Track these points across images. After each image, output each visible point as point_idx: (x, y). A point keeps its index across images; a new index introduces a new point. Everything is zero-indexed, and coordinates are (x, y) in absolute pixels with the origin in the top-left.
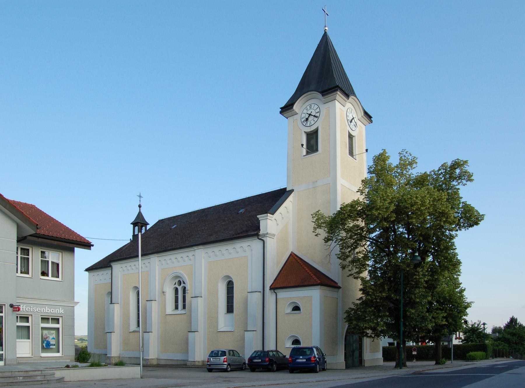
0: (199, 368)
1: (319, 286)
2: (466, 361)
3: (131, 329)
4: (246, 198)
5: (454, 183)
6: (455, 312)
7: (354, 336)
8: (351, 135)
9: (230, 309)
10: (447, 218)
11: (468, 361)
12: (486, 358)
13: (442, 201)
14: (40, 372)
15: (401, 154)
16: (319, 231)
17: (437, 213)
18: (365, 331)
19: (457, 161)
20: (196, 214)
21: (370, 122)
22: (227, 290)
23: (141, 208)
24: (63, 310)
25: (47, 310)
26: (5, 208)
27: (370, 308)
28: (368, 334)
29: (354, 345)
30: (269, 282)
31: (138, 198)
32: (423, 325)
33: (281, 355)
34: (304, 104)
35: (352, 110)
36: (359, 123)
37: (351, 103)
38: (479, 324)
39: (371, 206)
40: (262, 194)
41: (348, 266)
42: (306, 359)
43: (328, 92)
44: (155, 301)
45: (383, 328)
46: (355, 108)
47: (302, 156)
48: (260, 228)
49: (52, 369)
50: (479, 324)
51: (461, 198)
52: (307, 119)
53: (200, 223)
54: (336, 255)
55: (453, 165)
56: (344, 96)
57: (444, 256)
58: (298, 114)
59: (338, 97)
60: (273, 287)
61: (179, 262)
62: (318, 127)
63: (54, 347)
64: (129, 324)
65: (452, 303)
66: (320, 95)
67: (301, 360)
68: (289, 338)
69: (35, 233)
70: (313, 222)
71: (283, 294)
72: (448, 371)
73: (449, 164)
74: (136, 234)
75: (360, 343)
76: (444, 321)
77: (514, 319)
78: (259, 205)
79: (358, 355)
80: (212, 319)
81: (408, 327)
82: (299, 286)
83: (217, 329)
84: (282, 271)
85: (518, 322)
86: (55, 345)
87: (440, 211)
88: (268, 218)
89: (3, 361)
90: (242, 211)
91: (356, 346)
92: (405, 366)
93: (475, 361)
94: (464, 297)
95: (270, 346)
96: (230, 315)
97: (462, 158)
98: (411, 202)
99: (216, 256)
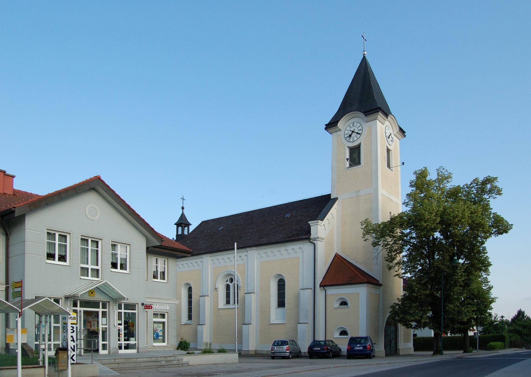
1: (366, 284)
2: (487, 351)
3: (182, 322)
4: (289, 203)
5: (486, 196)
6: (482, 307)
7: (391, 327)
8: (389, 149)
9: (281, 303)
10: (483, 228)
12: (504, 348)
13: (478, 213)
14: (174, 358)
15: (439, 170)
16: (368, 236)
17: (475, 224)
18: (410, 323)
19: (488, 177)
22: (278, 287)
24: (169, 307)
26: (141, 225)
27: (415, 303)
28: (412, 325)
29: (391, 335)
30: (319, 280)
32: (460, 318)
33: (334, 345)
34: (347, 122)
36: (395, 138)
38: (496, 317)
39: (419, 218)
40: (304, 200)
41: (394, 267)
42: (363, 347)
45: (426, 321)
46: (391, 124)
47: (346, 168)
48: (311, 233)
49: (181, 355)
50: (496, 317)
51: (491, 209)
52: (350, 136)
53: (247, 226)
54: (385, 258)
55: (485, 181)
56: (384, 116)
57: (477, 259)
58: (341, 130)
59: (379, 117)
60: (323, 285)
63: (161, 338)
64: (181, 317)
65: (479, 298)
66: (362, 115)
67: (358, 348)
68: (337, 329)
69: (160, 244)
70: (362, 228)
71: (332, 291)
72: (488, 356)
73: (481, 179)
74: (179, 234)
75: (396, 333)
76: (474, 314)
77: (522, 312)
78: (304, 210)
79: (394, 345)
80: (264, 312)
83: (270, 322)
84: (329, 271)
85: (525, 315)
87: (477, 222)
88: (319, 224)
89: (107, 350)
90: (288, 215)
92: (442, 354)
93: (496, 350)
94: (490, 293)
95: (321, 337)
96: (281, 309)
97: (493, 175)
98: (454, 215)
99: (268, 256)
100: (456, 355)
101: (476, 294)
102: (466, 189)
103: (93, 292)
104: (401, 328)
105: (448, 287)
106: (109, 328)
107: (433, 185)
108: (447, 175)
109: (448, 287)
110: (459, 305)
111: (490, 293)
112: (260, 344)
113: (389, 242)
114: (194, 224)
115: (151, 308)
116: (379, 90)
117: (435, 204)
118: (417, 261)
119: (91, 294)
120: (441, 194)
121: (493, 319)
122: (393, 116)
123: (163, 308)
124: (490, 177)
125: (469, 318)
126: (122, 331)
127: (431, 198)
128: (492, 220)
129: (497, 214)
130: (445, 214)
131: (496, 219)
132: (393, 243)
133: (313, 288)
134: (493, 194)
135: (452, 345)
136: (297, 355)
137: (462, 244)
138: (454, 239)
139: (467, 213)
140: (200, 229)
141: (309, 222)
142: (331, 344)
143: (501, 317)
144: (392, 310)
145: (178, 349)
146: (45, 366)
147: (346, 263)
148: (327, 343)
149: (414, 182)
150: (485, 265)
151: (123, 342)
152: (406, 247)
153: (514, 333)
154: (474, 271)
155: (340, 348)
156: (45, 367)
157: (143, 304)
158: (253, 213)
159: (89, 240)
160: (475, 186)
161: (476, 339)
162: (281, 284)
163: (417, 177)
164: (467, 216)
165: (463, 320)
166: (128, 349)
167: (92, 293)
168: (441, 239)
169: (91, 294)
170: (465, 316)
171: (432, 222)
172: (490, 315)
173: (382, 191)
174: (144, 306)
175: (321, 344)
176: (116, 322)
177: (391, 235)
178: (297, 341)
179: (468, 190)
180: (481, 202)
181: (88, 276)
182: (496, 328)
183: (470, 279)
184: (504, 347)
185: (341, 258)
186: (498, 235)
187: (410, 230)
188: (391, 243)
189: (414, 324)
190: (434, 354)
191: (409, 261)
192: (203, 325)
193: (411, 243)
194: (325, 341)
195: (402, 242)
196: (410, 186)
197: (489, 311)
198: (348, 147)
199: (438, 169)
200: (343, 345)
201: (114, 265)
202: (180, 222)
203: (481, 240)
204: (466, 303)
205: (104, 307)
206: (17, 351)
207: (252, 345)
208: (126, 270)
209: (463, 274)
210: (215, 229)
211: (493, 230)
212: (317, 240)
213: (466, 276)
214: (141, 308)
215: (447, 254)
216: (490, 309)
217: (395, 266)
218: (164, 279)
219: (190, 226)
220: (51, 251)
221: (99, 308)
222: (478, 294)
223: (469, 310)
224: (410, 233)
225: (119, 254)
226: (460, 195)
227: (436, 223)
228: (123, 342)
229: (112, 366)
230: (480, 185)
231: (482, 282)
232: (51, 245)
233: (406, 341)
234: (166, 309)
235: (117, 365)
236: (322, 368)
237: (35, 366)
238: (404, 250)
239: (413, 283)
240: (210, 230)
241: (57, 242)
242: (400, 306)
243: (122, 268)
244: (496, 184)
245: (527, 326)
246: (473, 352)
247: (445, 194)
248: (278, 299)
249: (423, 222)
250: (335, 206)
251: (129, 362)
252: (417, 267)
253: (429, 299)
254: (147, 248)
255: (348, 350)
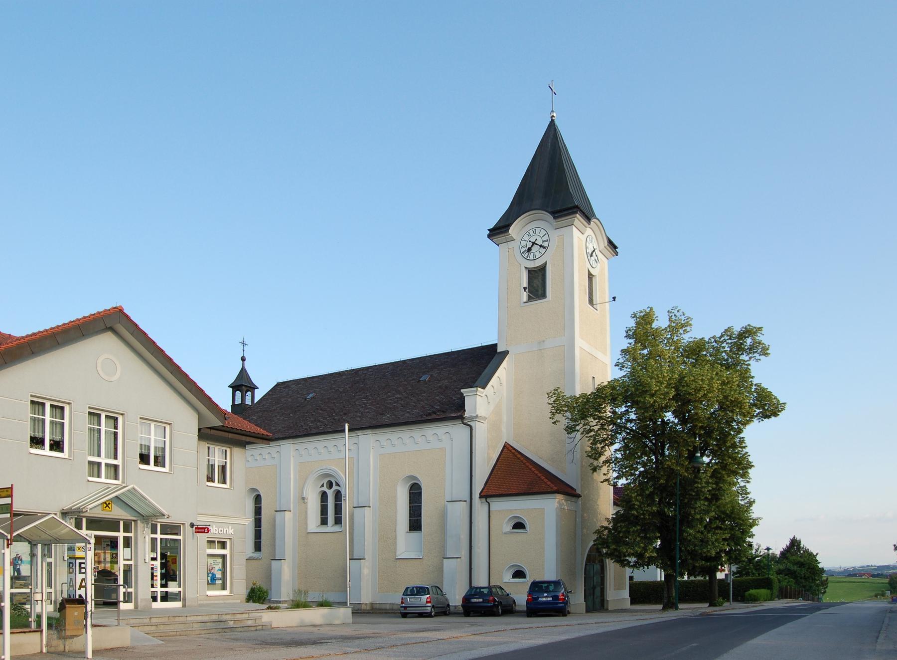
0: (370, 613)
5: (744, 357)
6: (738, 534)
7: (595, 565)
8: (591, 274)
9: (415, 525)
10: (741, 408)
11: (747, 602)
14: (247, 615)
16: (558, 417)
19: (748, 327)
20: (344, 377)
21: (615, 253)
23: (245, 362)
24: (232, 530)
25: (214, 530)
27: (635, 526)
28: (630, 562)
29: (595, 578)
30: (478, 487)
31: (241, 346)
32: (705, 550)
35: (592, 238)
36: (600, 256)
37: (592, 229)
38: (758, 549)
43: (562, 214)
44: (290, 512)
46: (594, 233)
50: (758, 549)
51: (753, 377)
52: (529, 250)
53: (357, 393)
54: (586, 452)
56: (584, 220)
59: (576, 222)
60: (485, 494)
61: (330, 452)
62: (546, 262)
63: (220, 582)
65: (734, 519)
66: (549, 217)
67: (545, 598)
69: (222, 425)
70: (549, 403)
71: (499, 505)
72: (746, 611)
73: (737, 329)
74: (236, 403)
75: (602, 575)
76: (726, 544)
77: (796, 540)
78: (452, 369)
80: (387, 540)
81: (683, 553)
82: (524, 493)
85: (802, 546)
86: (221, 580)
87: (732, 399)
88: (478, 394)
90: (426, 377)
91: (597, 579)
92: (677, 608)
93: (759, 602)
94: (750, 511)
95: (481, 581)
96: (415, 535)
98: (696, 386)
100: (699, 610)
101: (728, 512)
102: (714, 344)
103: (109, 503)
104: (611, 565)
105: (686, 500)
106: (136, 566)
107: (662, 336)
108: (684, 320)
109: (686, 500)
110: (703, 529)
111: (750, 511)
112: (379, 592)
113: (593, 426)
114: (263, 388)
115: (208, 532)
116: (577, 177)
117: (666, 368)
118: (636, 458)
119: (105, 508)
120: (675, 352)
121: (754, 551)
122: (599, 220)
123: (223, 531)
124: (751, 327)
125: (718, 550)
126: (157, 571)
127: (660, 358)
128: (753, 396)
129: (762, 386)
130: (683, 384)
131: (761, 395)
132: (599, 429)
133: (468, 500)
134: (755, 355)
135: (691, 594)
136: (443, 610)
137: (709, 433)
138: (695, 424)
139: (717, 383)
140: (274, 396)
141: (462, 391)
142: (500, 593)
143: (765, 549)
144: (597, 538)
145: (248, 600)
146: (42, 630)
147: (522, 459)
148: (494, 590)
149: (633, 331)
150: (742, 466)
151: (159, 590)
152: (620, 436)
153: (786, 575)
154: (726, 476)
155: (513, 599)
156: (42, 631)
157: (192, 525)
158: (366, 372)
159: (46, 404)
160: (727, 340)
161: (729, 584)
162: (415, 493)
163: (637, 323)
164: (717, 389)
165: (709, 554)
166: (167, 601)
167: (107, 506)
168: (676, 425)
169: (105, 508)
170: (713, 548)
171: (662, 397)
172: (750, 545)
173: (580, 343)
174: (194, 528)
175: (483, 592)
176: (147, 555)
177: (596, 415)
178: (443, 588)
179: (716, 345)
180: (737, 365)
181: (99, 476)
182: (758, 567)
183: (720, 489)
184: (772, 597)
185: (513, 451)
186: (763, 419)
187: (627, 408)
188: (596, 428)
189: (633, 560)
190: (664, 609)
191: (625, 457)
192: (281, 560)
193: (628, 429)
194: (490, 588)
195: (613, 427)
196: (626, 337)
197: (748, 539)
198: (526, 268)
199: (670, 311)
200: (520, 595)
201: (144, 459)
202: (239, 383)
203: (736, 427)
204: (713, 527)
205: (127, 529)
206: (2, 604)
207: (366, 598)
208: (164, 466)
209: (710, 481)
210: (300, 397)
211: (755, 411)
212: (474, 420)
213: (714, 484)
214: (190, 531)
215: (685, 448)
216: (750, 537)
217: (602, 466)
218: (224, 482)
219: (256, 390)
220: (37, 433)
221: (119, 532)
222: (732, 512)
223: (718, 537)
224: (627, 412)
225: (104, 431)
226: (704, 353)
227: (668, 398)
228: (159, 590)
229: (147, 629)
230: (735, 338)
231: (739, 493)
232: (39, 423)
233: (619, 587)
234: (228, 533)
235: (154, 628)
236: (493, 631)
237: (25, 631)
238: (616, 441)
239: (632, 493)
240: (292, 398)
241: (48, 418)
242: (610, 530)
243: (156, 463)
244: (760, 337)
245: (805, 563)
246: (724, 605)
247: (681, 350)
248: (410, 517)
249: (648, 396)
250: (504, 364)
251: (175, 623)
252: (637, 467)
253: (656, 521)
254: (199, 430)
255: (528, 602)
